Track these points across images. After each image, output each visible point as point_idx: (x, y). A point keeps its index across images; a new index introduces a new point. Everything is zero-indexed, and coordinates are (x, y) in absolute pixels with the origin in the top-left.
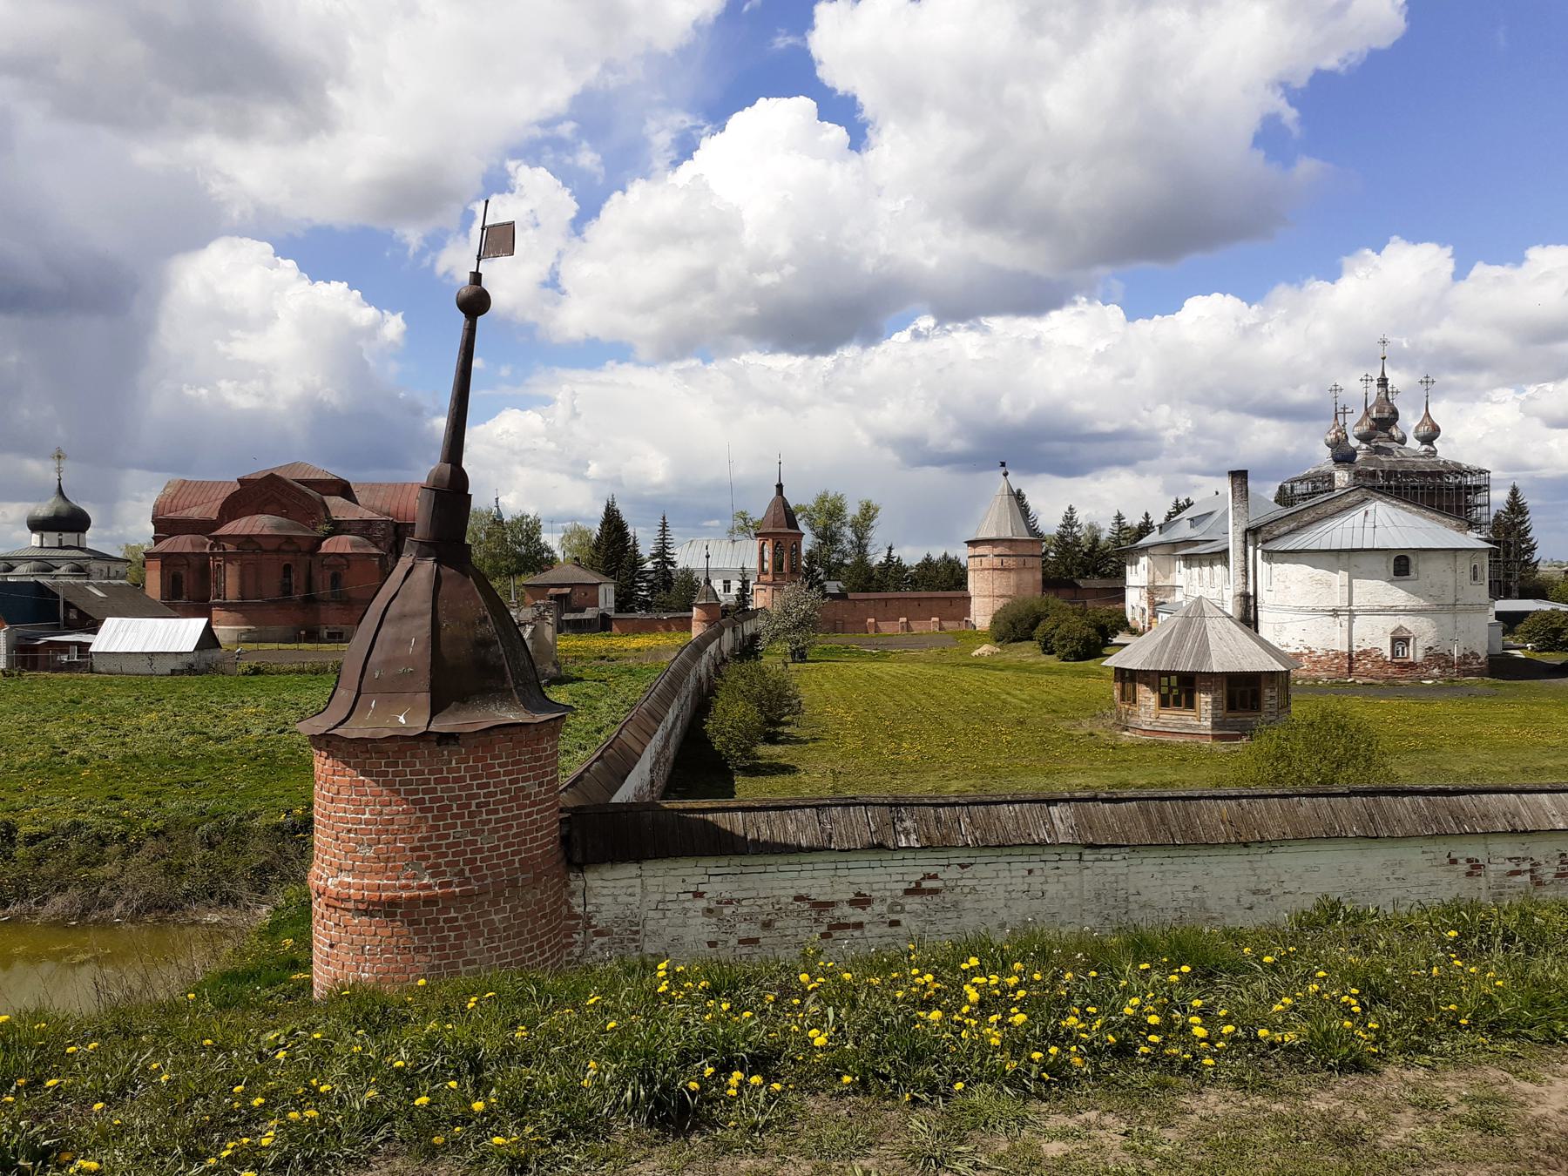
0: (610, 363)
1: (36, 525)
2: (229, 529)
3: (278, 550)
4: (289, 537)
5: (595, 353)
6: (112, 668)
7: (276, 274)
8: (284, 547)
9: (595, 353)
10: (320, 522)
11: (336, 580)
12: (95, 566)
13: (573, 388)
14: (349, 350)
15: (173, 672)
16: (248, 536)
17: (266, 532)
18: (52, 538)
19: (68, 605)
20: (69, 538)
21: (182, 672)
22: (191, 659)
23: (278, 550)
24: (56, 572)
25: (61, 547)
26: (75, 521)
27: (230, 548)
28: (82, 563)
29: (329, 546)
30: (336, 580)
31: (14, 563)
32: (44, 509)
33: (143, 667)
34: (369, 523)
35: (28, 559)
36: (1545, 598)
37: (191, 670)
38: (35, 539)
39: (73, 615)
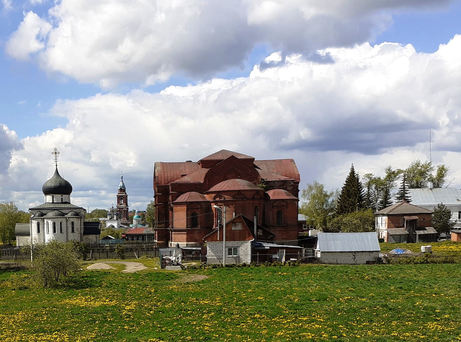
0: (98, 95)
1: (47, 191)
3: (253, 199)
5: (83, 89)
11: (279, 213)
15: (368, 263)
18: (58, 198)
21: (373, 263)
23: (253, 199)
24: (66, 216)
27: (228, 198)
29: (271, 193)
30: (279, 213)
31: (44, 212)
38: (49, 198)
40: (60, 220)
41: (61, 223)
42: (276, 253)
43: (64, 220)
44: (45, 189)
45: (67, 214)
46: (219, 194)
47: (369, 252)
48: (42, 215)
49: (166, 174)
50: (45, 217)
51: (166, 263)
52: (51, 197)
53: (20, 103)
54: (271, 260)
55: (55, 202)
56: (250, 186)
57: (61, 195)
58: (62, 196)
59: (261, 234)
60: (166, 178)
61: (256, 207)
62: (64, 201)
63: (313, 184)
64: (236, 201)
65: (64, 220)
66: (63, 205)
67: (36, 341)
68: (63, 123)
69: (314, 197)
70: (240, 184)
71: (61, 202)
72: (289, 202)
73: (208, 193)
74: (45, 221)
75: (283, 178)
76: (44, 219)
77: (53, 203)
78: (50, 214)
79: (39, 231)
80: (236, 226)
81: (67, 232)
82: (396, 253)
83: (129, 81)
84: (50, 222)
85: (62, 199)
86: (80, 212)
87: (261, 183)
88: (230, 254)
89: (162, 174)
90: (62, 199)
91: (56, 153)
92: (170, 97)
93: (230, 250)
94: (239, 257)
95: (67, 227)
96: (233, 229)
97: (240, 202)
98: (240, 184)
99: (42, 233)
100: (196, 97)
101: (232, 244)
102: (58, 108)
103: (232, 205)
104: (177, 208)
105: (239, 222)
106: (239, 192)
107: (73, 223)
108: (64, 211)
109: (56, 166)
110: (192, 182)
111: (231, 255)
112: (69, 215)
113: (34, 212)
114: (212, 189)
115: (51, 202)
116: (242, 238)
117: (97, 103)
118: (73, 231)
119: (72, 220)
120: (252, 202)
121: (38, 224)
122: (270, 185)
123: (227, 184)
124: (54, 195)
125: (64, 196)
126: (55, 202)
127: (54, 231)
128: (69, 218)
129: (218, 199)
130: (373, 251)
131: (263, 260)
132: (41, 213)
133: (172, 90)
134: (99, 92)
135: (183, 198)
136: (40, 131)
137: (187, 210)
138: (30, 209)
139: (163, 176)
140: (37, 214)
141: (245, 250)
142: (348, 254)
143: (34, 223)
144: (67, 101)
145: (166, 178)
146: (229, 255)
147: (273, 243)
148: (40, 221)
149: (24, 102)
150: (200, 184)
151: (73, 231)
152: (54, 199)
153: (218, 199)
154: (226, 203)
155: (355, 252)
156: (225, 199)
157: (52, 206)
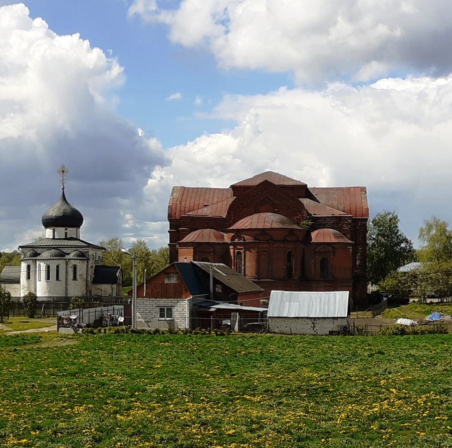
0: (283, 89)
1: (49, 223)
2: (244, 223)
3: (284, 240)
4: (292, 230)
5: (264, 80)
6: (283, 329)
7: (31, 34)
8: (288, 238)
9: (264, 80)
10: (303, 219)
11: (324, 262)
12: (91, 252)
13: (261, 108)
14: (79, 90)
15: (331, 333)
16: (264, 230)
17: (275, 226)
18: (61, 232)
19: (216, 282)
20: (71, 232)
21: (338, 333)
22: (344, 323)
23: (284, 240)
24: (67, 257)
25: (66, 239)
26: (71, 219)
27: (248, 239)
28: (83, 250)
29: (316, 236)
30: (324, 262)
31: (39, 251)
32: (54, 211)
33: (307, 328)
34: (339, 219)
35: (49, 248)
36: (208, 262)
37: (345, 331)
38: (49, 233)
39: (219, 289)
40: (56, 263)
41: (58, 267)
42: (229, 317)
43: (62, 264)
44: (44, 218)
45: (68, 254)
46: (238, 233)
47: (334, 318)
48: (36, 254)
49: (183, 203)
50: (38, 258)
51: (63, 324)
52: (51, 231)
53: (172, 97)
54: (218, 325)
55: (56, 237)
56: (282, 222)
57: (64, 229)
58: (66, 229)
59: (220, 291)
60: (183, 209)
61: (290, 253)
62: (68, 237)
63: (432, 222)
64: (259, 243)
65: (62, 264)
66: (67, 241)
67: (1, 425)
68: (229, 126)
69: (432, 240)
70: (268, 220)
71: (64, 237)
72: (334, 245)
73: (227, 232)
74: (37, 262)
75: (338, 213)
76: (36, 260)
77: (54, 238)
78: (46, 254)
79: (29, 278)
80: (169, 278)
81: (66, 279)
82: (430, 320)
83: (335, 70)
84: (43, 266)
85: (66, 233)
86: (87, 252)
87: (307, 219)
88: (162, 316)
89: (179, 202)
90: (66, 233)
91: (63, 171)
92: (386, 93)
93: (162, 310)
94: (173, 320)
95: (67, 272)
96: (166, 281)
97: (265, 246)
98: (268, 220)
99: (33, 279)
100: (422, 96)
101: (164, 302)
102: (226, 107)
103: (253, 248)
104: (183, 250)
105: (173, 273)
106: (264, 231)
107: (75, 267)
108: (65, 250)
109: (63, 189)
110: (210, 216)
111: (164, 317)
112: (71, 256)
113: (26, 250)
114: (235, 227)
115: (51, 237)
116: (177, 293)
117: (285, 100)
118: (75, 278)
119: (73, 262)
120: (282, 245)
121: (29, 267)
122: (319, 223)
123: (251, 220)
124: (56, 229)
125: (69, 229)
126: (56, 237)
127: (48, 278)
128: (70, 259)
129: (236, 240)
130: (338, 318)
131: (205, 325)
132: (34, 252)
133: (384, 84)
134: (283, 85)
135: (190, 237)
136: (192, 136)
137: (194, 253)
138: (20, 247)
139: (179, 206)
140: (29, 254)
141: (182, 311)
142: (306, 320)
143: (24, 266)
144: (240, 97)
145: (183, 209)
146: (161, 317)
147: (236, 303)
148: (30, 262)
149: (178, 96)
150: (222, 219)
151: (75, 278)
152: (56, 233)
153: (236, 240)
154: (247, 246)
155: (315, 318)
156: (244, 240)
157: (52, 243)
